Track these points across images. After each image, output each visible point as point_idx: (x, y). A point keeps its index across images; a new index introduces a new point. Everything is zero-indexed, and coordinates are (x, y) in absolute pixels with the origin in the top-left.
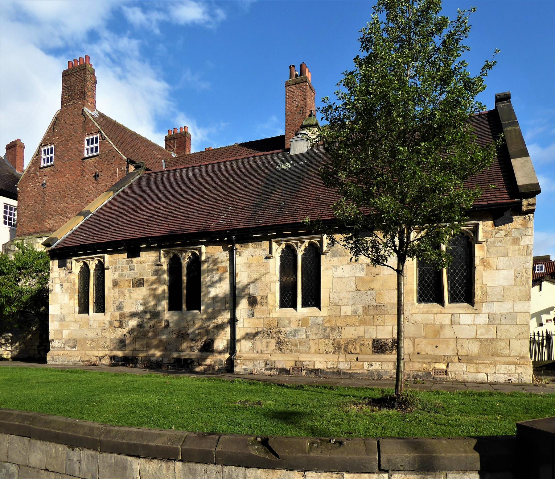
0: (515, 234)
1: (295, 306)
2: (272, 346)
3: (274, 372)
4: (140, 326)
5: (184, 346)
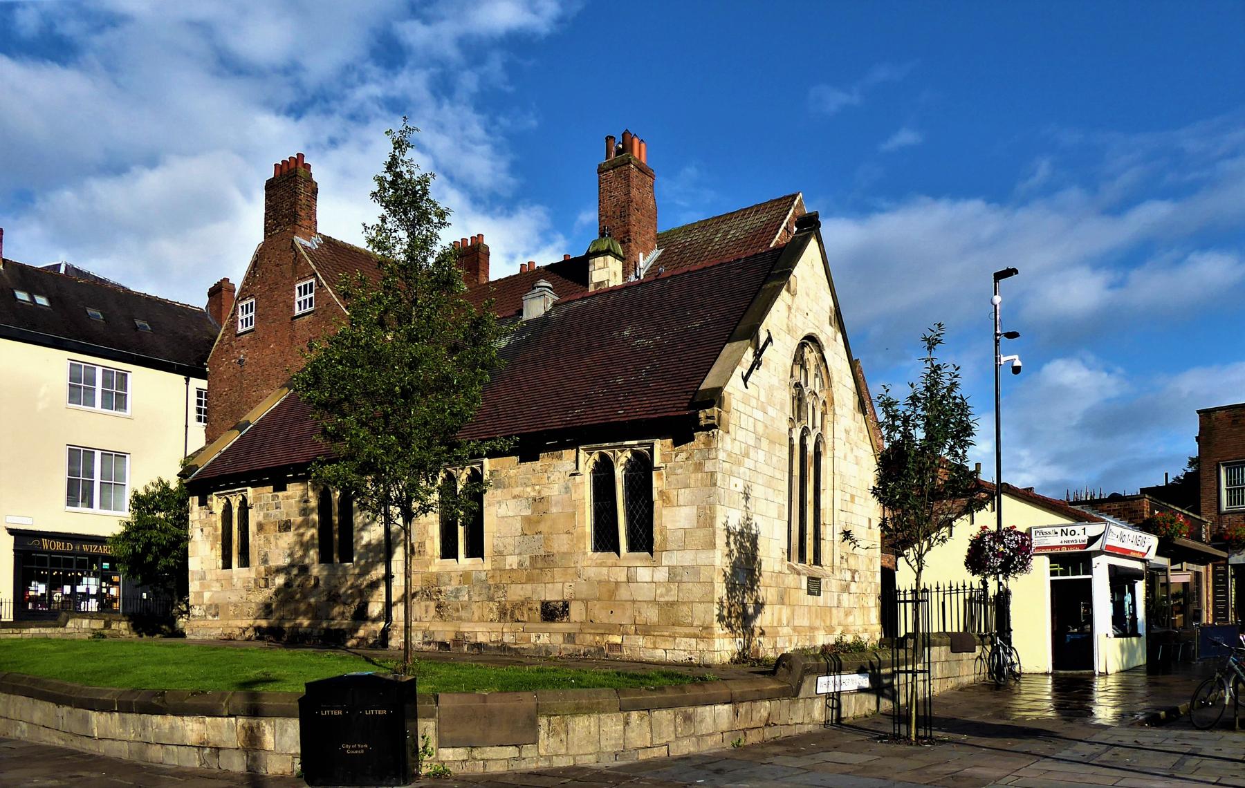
0: (697, 456)
1: (455, 556)
2: (432, 612)
3: (432, 647)
4: (288, 585)
5: (337, 610)
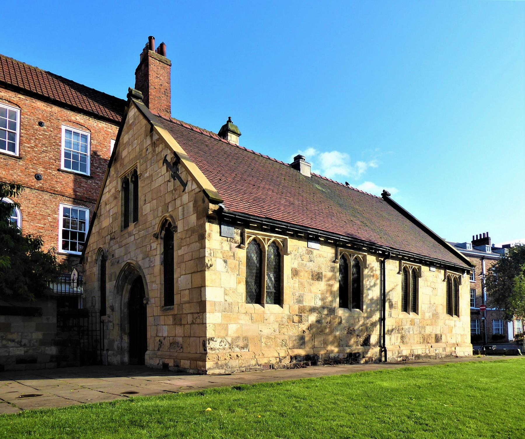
2: (399, 340)
